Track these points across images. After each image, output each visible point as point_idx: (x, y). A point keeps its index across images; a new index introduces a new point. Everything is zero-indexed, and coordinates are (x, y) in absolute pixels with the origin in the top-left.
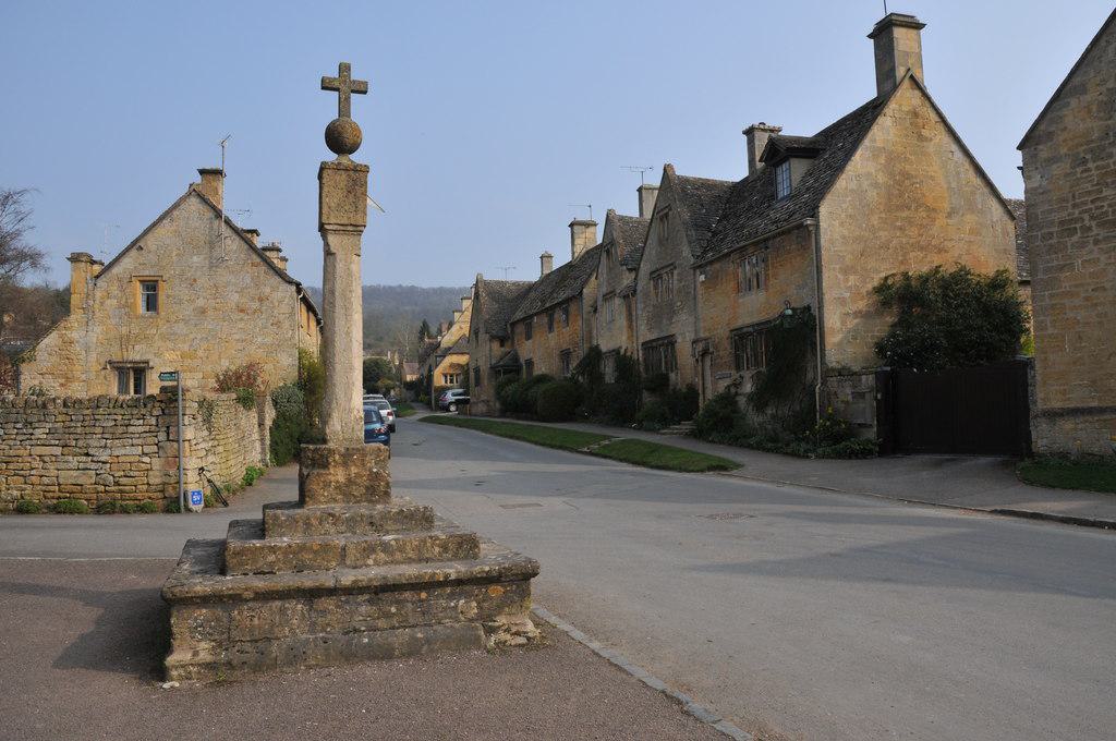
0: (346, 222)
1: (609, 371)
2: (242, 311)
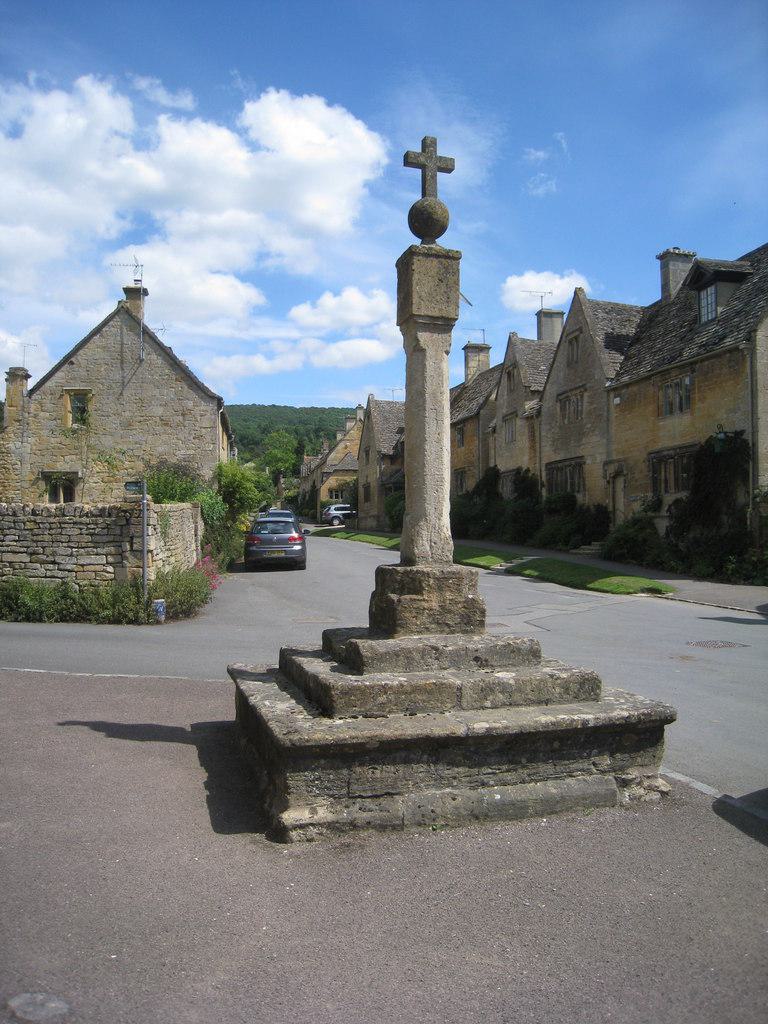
1: (506, 489)
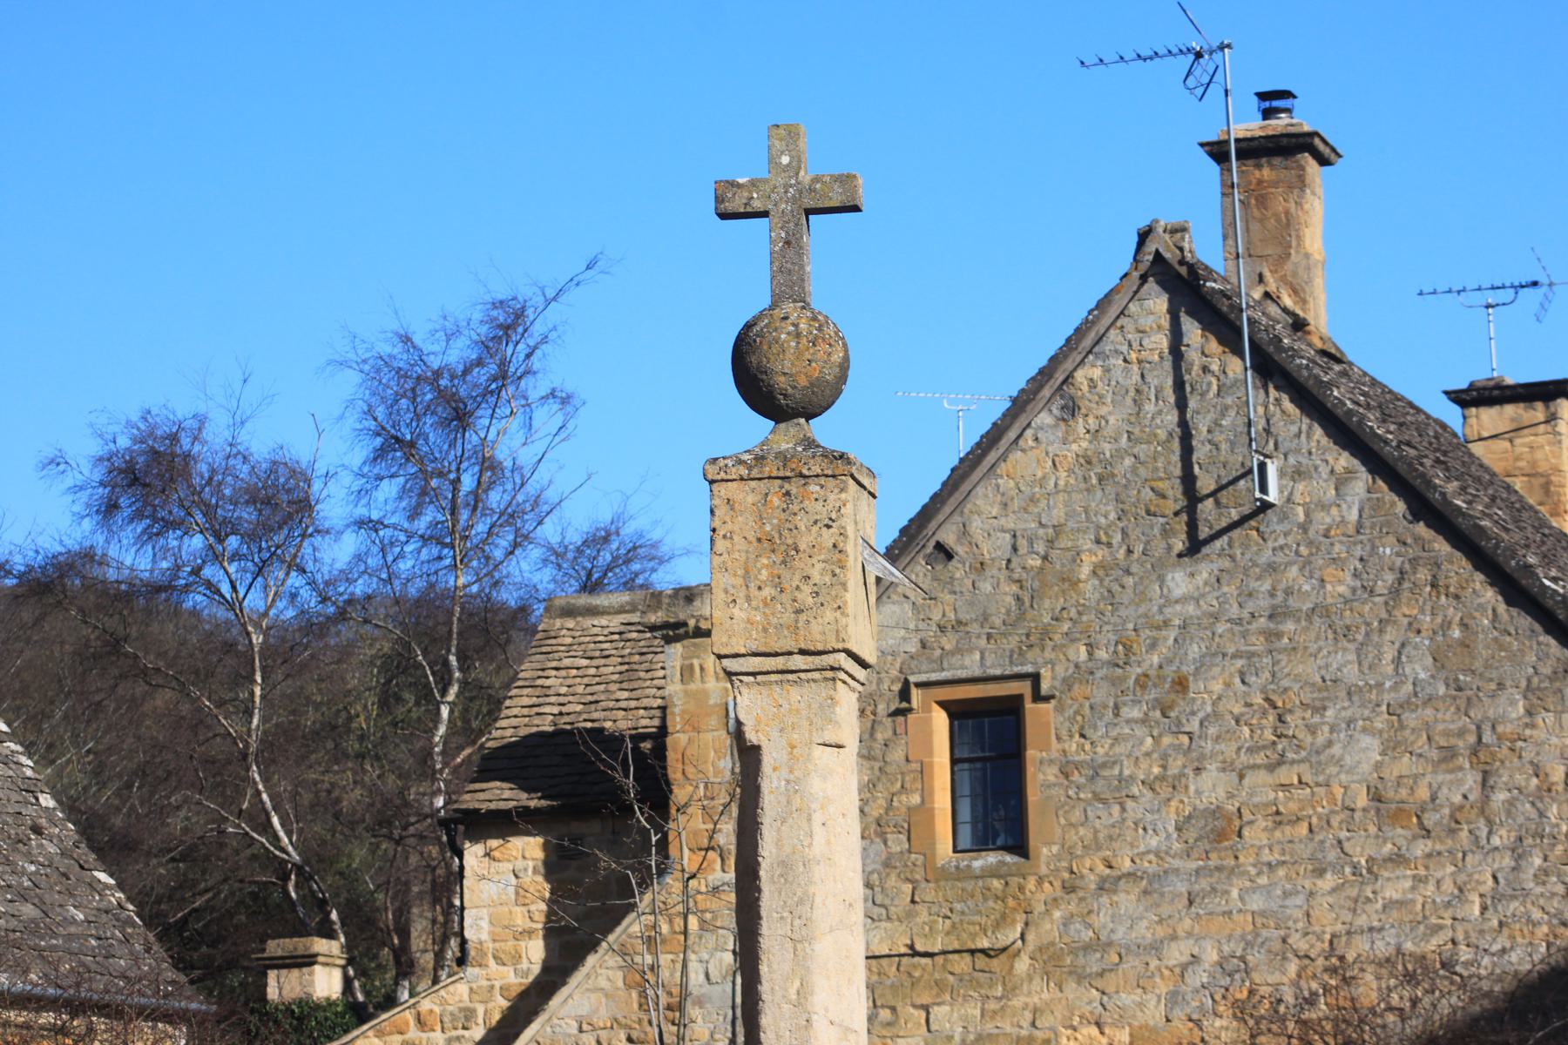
0: (789, 644)
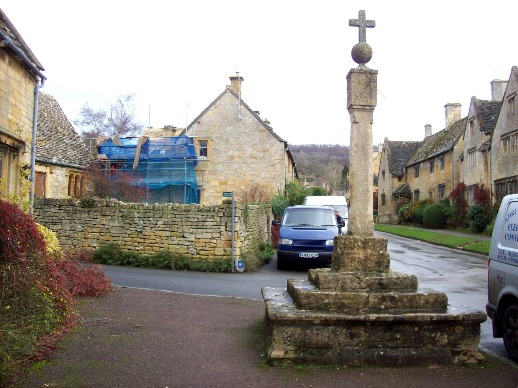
1: (470, 199)
2: (254, 158)
